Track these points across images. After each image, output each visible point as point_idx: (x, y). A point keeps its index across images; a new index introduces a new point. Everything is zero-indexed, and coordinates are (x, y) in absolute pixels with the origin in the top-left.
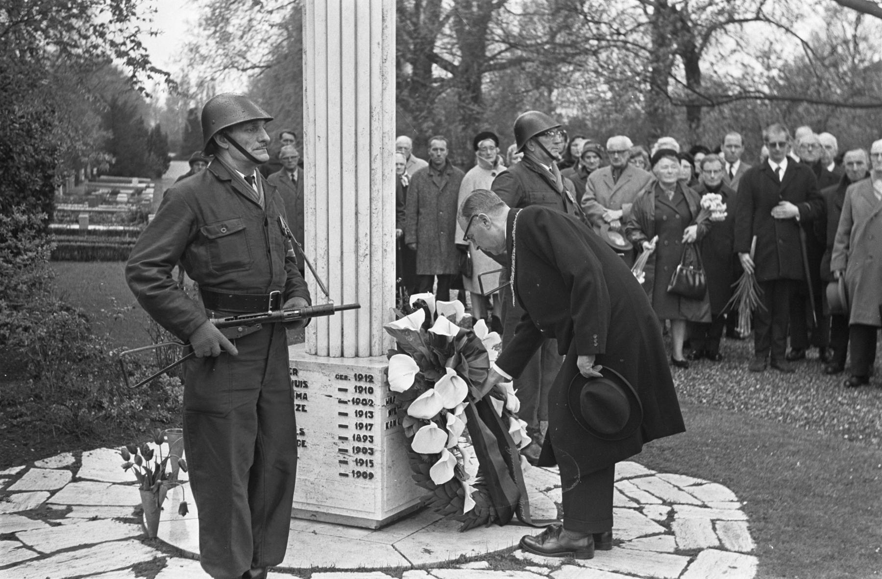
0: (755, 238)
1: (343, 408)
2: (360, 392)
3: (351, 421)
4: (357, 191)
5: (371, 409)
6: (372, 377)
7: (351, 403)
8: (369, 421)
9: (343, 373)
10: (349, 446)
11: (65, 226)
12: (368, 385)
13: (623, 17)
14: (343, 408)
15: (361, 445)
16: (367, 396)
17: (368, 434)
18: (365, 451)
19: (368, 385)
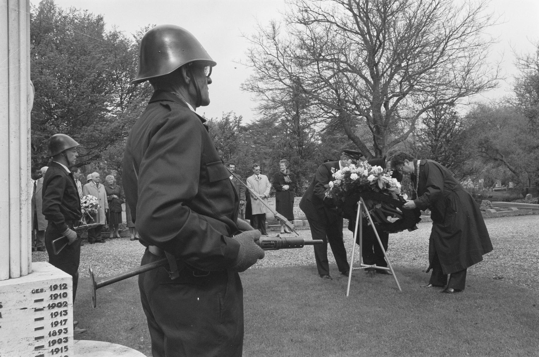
0: (348, 295)
1: (39, 315)
2: (55, 298)
3: (47, 323)
4: (9, 124)
5: (65, 309)
6: (66, 285)
7: (47, 309)
8: (64, 318)
9: (39, 288)
10: (44, 343)
11: (153, 158)
12: (62, 292)
13: (363, 168)
14: (39, 315)
15: (56, 338)
16: (62, 300)
17: (62, 327)
18: (60, 341)
19: (62, 292)
